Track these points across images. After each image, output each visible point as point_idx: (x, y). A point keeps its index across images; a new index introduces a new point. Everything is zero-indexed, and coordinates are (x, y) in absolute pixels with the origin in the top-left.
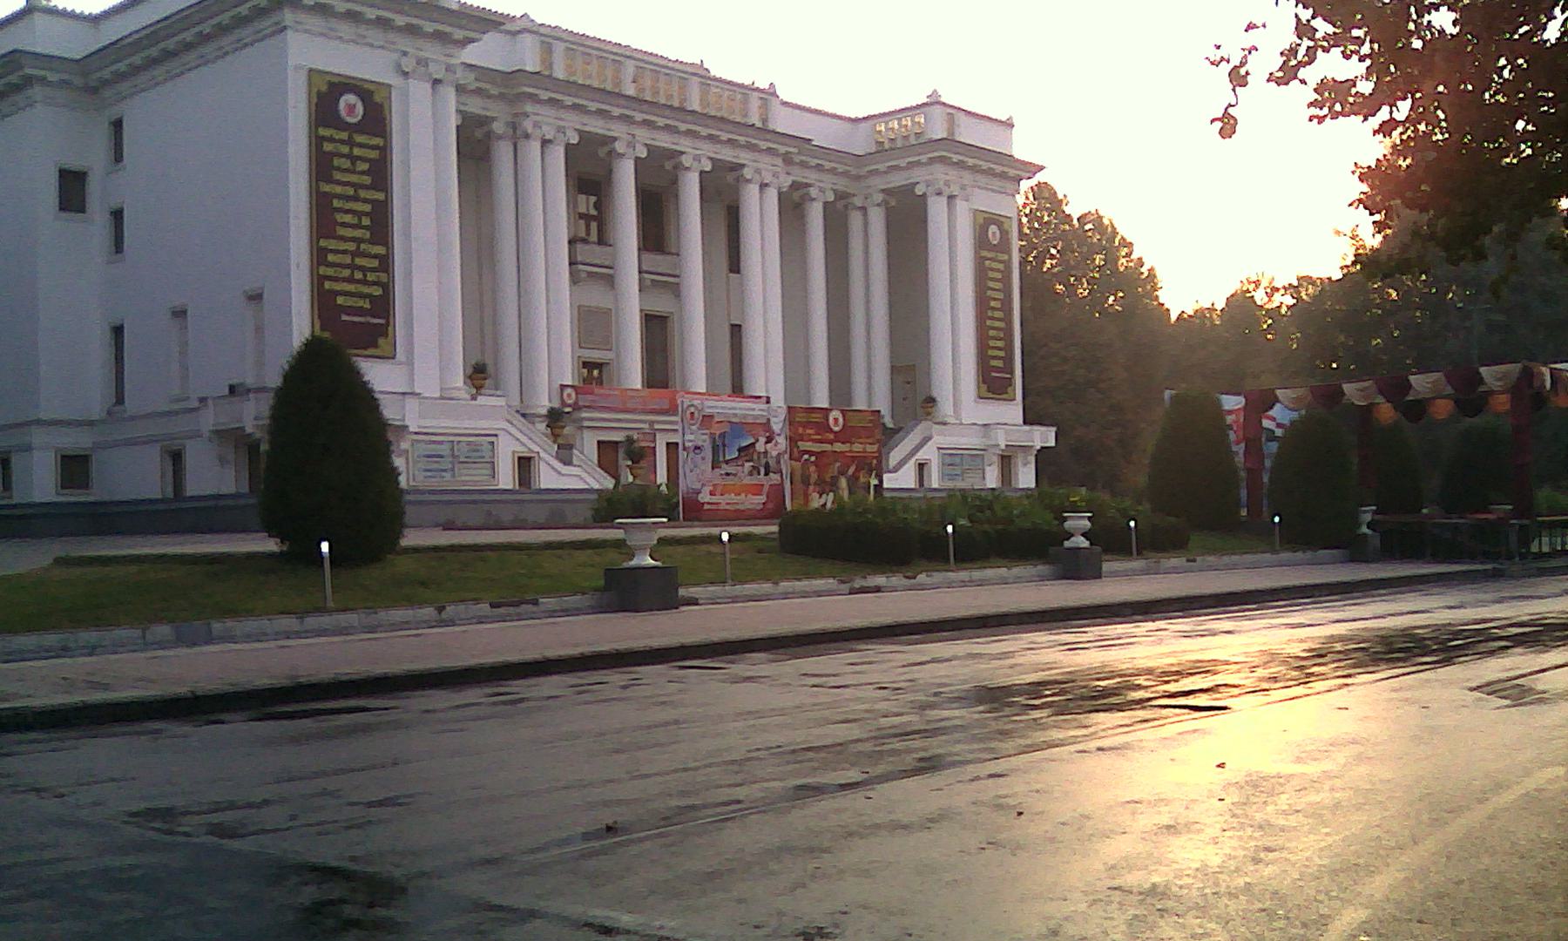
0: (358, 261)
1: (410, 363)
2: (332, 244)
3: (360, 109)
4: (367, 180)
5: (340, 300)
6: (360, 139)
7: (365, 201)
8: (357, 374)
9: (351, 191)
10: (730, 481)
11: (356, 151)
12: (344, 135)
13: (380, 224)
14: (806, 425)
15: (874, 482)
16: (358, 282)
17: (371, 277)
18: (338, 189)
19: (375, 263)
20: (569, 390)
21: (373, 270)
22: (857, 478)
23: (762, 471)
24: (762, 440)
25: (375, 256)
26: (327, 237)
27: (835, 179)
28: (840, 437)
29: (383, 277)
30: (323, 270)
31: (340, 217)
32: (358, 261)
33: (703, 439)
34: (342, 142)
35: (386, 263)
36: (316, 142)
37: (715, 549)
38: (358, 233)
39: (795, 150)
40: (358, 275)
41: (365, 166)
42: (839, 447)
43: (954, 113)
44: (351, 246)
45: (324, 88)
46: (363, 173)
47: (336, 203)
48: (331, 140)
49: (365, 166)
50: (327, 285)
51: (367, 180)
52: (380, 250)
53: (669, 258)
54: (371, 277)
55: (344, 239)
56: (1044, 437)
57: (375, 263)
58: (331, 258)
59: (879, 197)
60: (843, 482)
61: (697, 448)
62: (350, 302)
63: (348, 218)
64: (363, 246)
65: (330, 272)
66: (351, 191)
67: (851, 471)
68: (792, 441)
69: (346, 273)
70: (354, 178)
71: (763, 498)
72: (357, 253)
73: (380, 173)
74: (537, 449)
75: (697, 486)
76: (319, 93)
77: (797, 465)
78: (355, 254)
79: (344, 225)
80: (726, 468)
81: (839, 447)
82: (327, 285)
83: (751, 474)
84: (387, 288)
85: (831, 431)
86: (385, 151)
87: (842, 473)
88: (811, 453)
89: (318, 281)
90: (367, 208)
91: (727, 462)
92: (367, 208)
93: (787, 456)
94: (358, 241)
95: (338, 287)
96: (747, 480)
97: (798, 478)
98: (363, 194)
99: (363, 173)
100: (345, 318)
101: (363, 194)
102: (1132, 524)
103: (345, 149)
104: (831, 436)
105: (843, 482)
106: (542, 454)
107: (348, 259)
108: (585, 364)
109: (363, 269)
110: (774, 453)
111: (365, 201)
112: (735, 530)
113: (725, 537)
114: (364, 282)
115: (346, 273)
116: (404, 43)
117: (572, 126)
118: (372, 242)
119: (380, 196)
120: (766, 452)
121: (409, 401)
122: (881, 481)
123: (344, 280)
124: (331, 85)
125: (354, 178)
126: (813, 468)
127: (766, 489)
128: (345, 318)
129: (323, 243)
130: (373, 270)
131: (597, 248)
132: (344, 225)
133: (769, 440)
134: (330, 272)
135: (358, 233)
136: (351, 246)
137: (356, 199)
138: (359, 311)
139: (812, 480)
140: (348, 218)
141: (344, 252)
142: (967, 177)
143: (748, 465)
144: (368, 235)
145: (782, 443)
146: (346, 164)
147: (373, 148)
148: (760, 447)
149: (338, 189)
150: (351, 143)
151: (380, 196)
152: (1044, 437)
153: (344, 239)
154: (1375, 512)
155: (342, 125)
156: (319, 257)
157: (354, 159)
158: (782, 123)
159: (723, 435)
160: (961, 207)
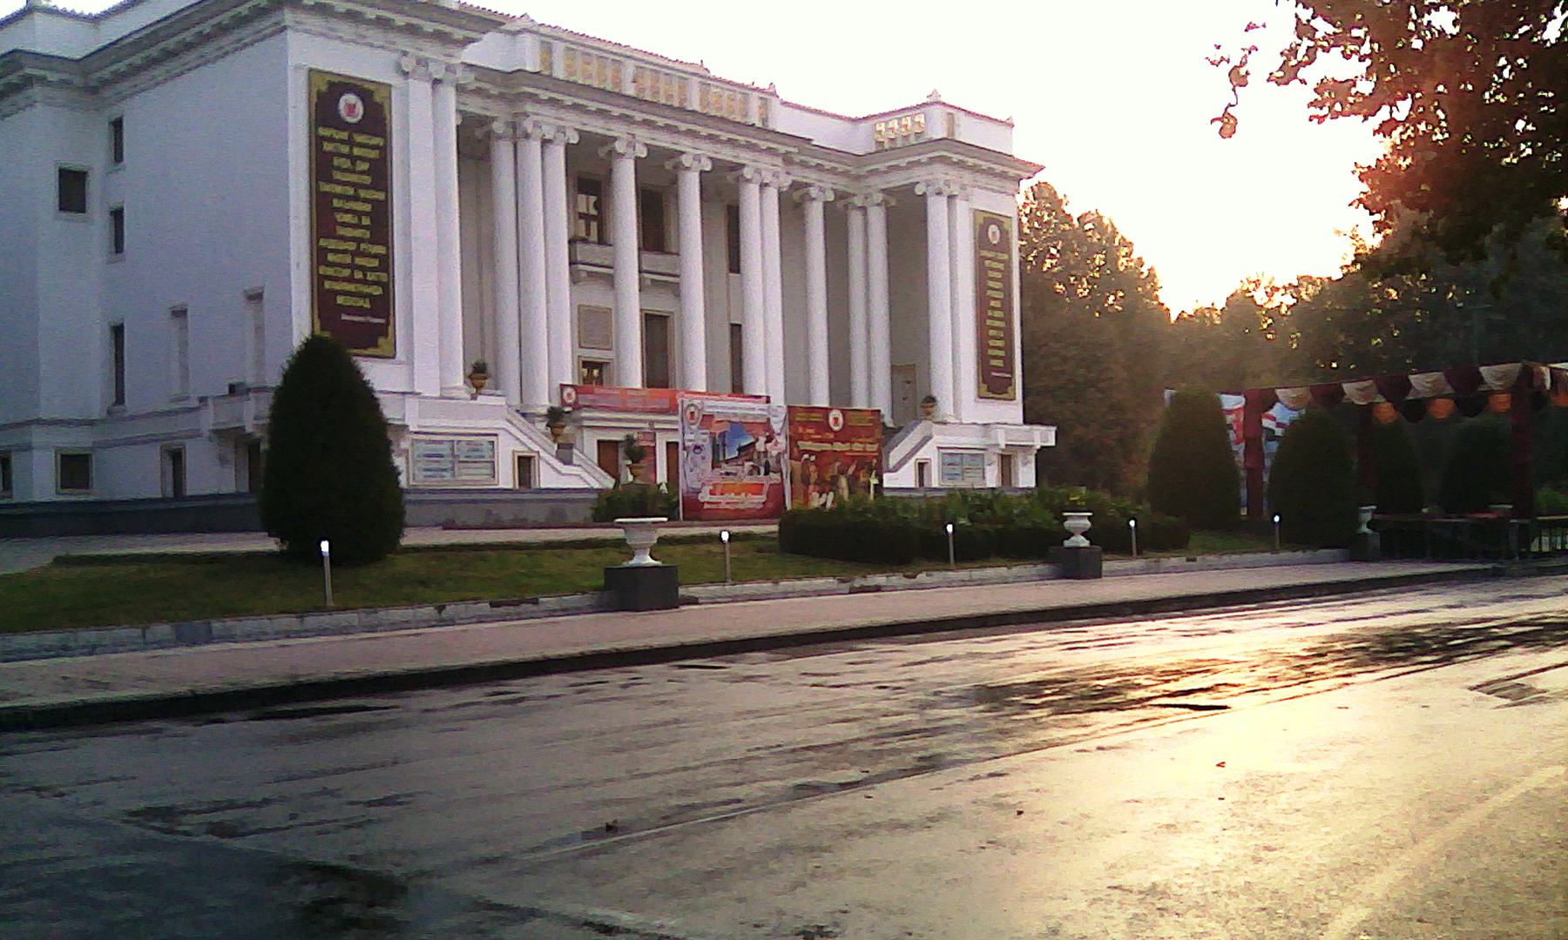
0: (358, 261)
1: (410, 362)
2: (332, 244)
3: (360, 109)
4: (367, 179)
5: (340, 300)
6: (359, 138)
7: (365, 201)
8: (357, 374)
9: (351, 191)
10: (730, 480)
11: (356, 151)
12: (344, 135)
13: (380, 223)
14: (805, 424)
15: (874, 481)
16: (358, 281)
17: (371, 277)
18: (338, 189)
19: (375, 263)
20: (569, 390)
21: (373, 270)
22: (857, 478)
23: (762, 470)
24: (762, 439)
25: (375, 256)
26: (328, 237)
27: (836, 179)
28: (841, 436)
29: (383, 277)
30: (323, 270)
31: (340, 217)
32: (358, 261)
33: (703, 438)
34: (342, 142)
35: (386, 263)
36: (316, 142)
37: (715, 548)
38: (358, 233)
39: (796, 149)
40: (358, 275)
41: (365, 166)
42: (839, 447)
43: (954, 112)
44: (351, 246)
45: (324, 88)
46: (363, 173)
47: (336, 203)
48: (331, 140)
49: (365, 166)
50: (327, 285)
51: (367, 179)
52: (380, 250)
53: (669, 257)
54: (371, 277)
55: (343, 239)
56: (1044, 436)
57: (375, 263)
58: (331, 257)
59: (879, 197)
60: (843, 482)
61: (697, 447)
62: (350, 302)
63: (348, 218)
64: (363, 246)
65: (330, 271)
66: (351, 191)
67: (851, 471)
68: (792, 440)
69: (346, 272)
70: (354, 178)
71: (763, 498)
72: (357, 253)
73: (380, 173)
74: (537, 448)
75: (697, 485)
76: (319, 93)
77: (797, 464)
78: (354, 254)
79: (344, 225)
80: (726, 468)
81: (839, 447)
82: (327, 285)
83: (751, 473)
84: (387, 288)
85: (831, 430)
86: (385, 151)
87: (842, 472)
88: (811, 453)
89: (318, 281)
90: (367, 207)
91: (727, 462)
92: (367, 207)
93: (787, 456)
94: (359, 240)
95: (337, 286)
96: (748, 480)
97: (798, 476)
98: (363, 193)
99: (363, 173)
100: (344, 317)
101: (363, 193)
102: (1132, 523)
103: (345, 149)
104: (832, 436)
105: (843, 482)
106: (542, 454)
107: (348, 259)
108: (585, 364)
109: (362, 268)
110: (774, 453)
111: (365, 201)
112: (735, 529)
113: (725, 536)
114: (364, 282)
115: (346, 272)
116: (403, 43)
117: (572, 126)
118: (372, 242)
119: (380, 196)
120: (766, 452)
121: (409, 400)
122: (881, 481)
123: (345, 280)
124: (331, 85)
125: (354, 178)
126: (812, 468)
127: (766, 489)
128: (344, 317)
129: (323, 243)
130: (373, 270)
131: (597, 248)
132: (344, 225)
133: (769, 440)
134: (330, 271)
135: (358, 233)
136: (351, 246)
137: (356, 198)
138: (359, 311)
139: (812, 480)
140: (348, 218)
141: (345, 252)
142: (967, 177)
143: (748, 464)
144: (368, 235)
145: (782, 442)
146: (346, 164)
147: (374, 147)
148: (760, 446)
149: (338, 189)
150: (351, 143)
151: (380, 196)
152: (1044, 436)
153: (343, 239)
154: (1374, 512)
155: (342, 125)
156: (319, 257)
157: (354, 159)
158: (783, 122)
159: (723, 435)
160: (961, 207)
